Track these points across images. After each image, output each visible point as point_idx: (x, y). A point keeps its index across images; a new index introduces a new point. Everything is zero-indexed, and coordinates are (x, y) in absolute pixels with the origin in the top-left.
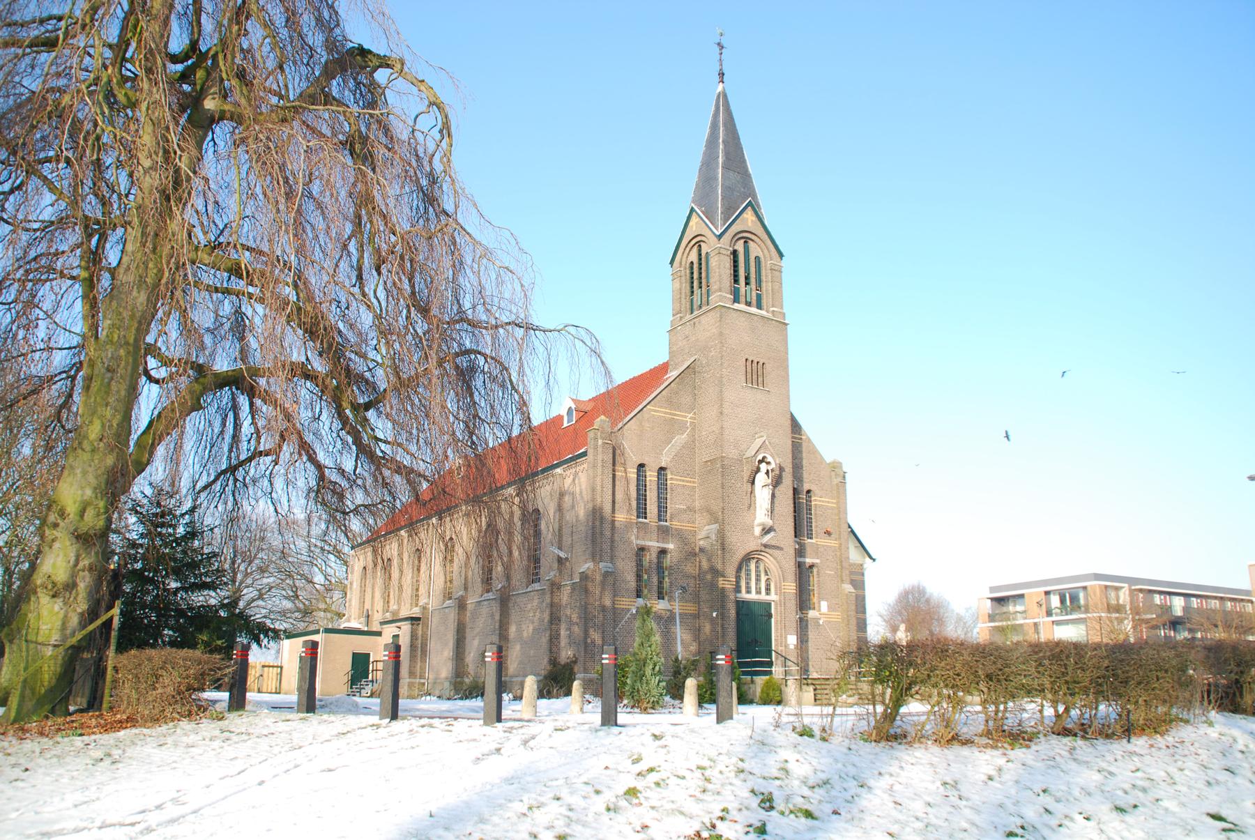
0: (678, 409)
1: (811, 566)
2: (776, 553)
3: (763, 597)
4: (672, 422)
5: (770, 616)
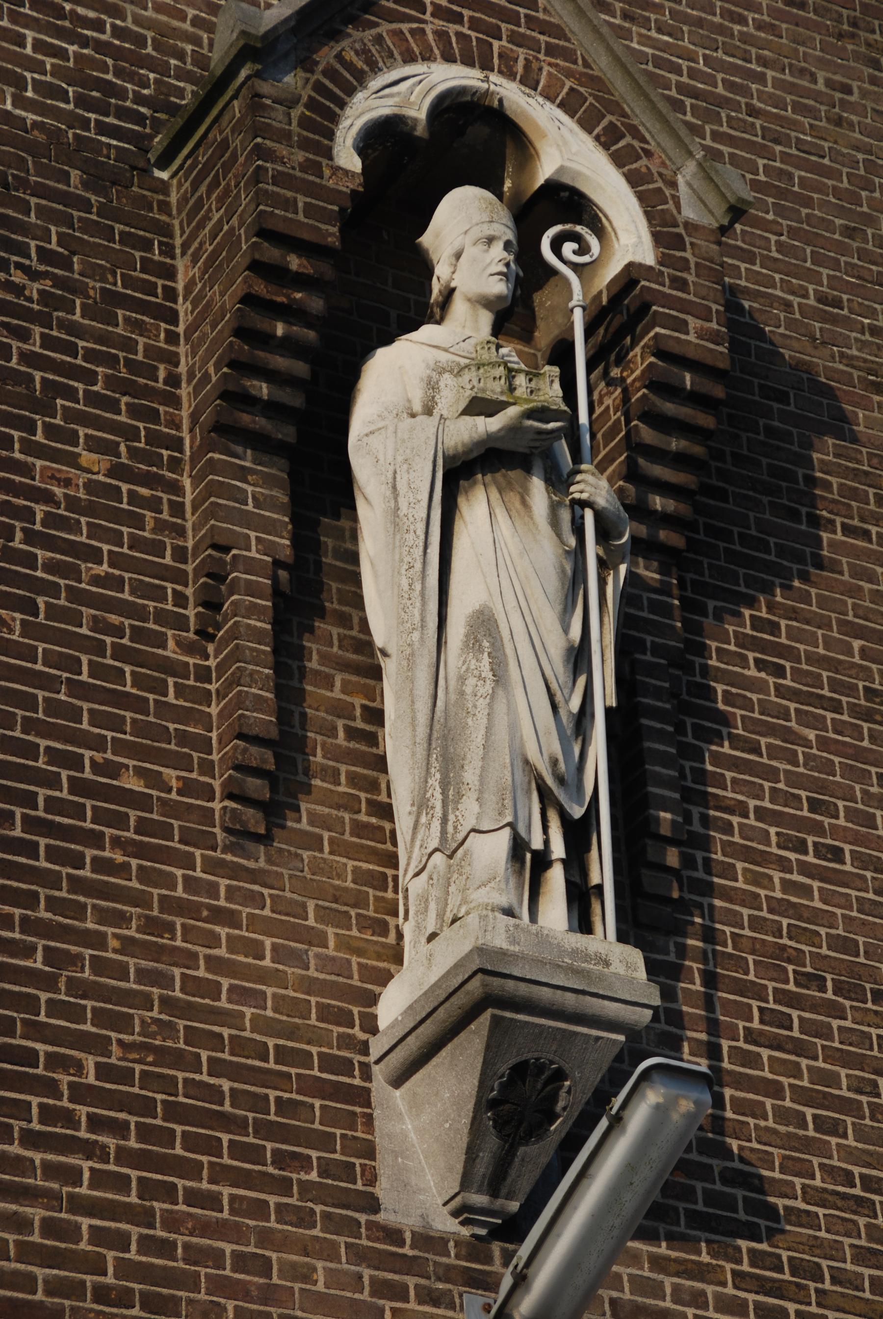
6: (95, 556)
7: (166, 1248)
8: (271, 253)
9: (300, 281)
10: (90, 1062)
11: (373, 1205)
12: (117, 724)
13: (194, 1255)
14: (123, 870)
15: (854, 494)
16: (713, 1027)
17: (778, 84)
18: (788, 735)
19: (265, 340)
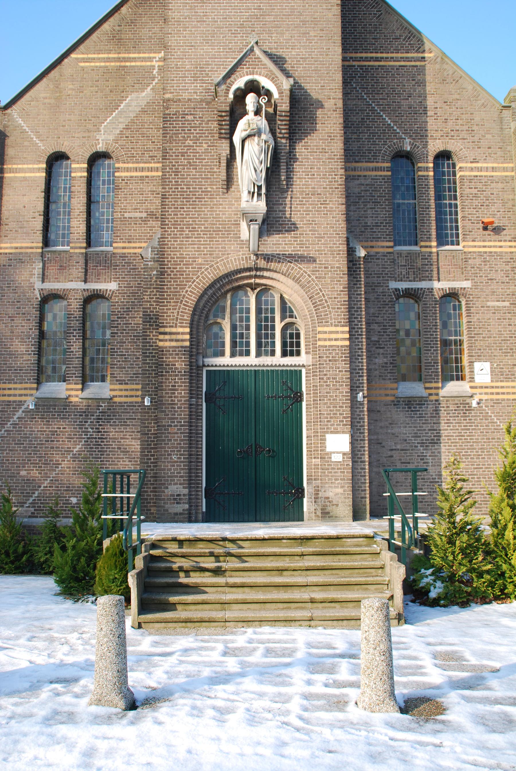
0: (136, 48)
1: (452, 295)
2: (296, 268)
3: (277, 360)
4: (122, 72)
5: (298, 398)
6: (205, 159)
7: (212, 248)
8: (220, 114)
9: (225, 116)
10: (203, 227)
11: (240, 238)
12: (207, 182)
13: (216, 248)
14: (208, 201)
15: (323, 117)
16: (291, 204)
17: (318, 52)
18: (308, 159)
19: (222, 125)
